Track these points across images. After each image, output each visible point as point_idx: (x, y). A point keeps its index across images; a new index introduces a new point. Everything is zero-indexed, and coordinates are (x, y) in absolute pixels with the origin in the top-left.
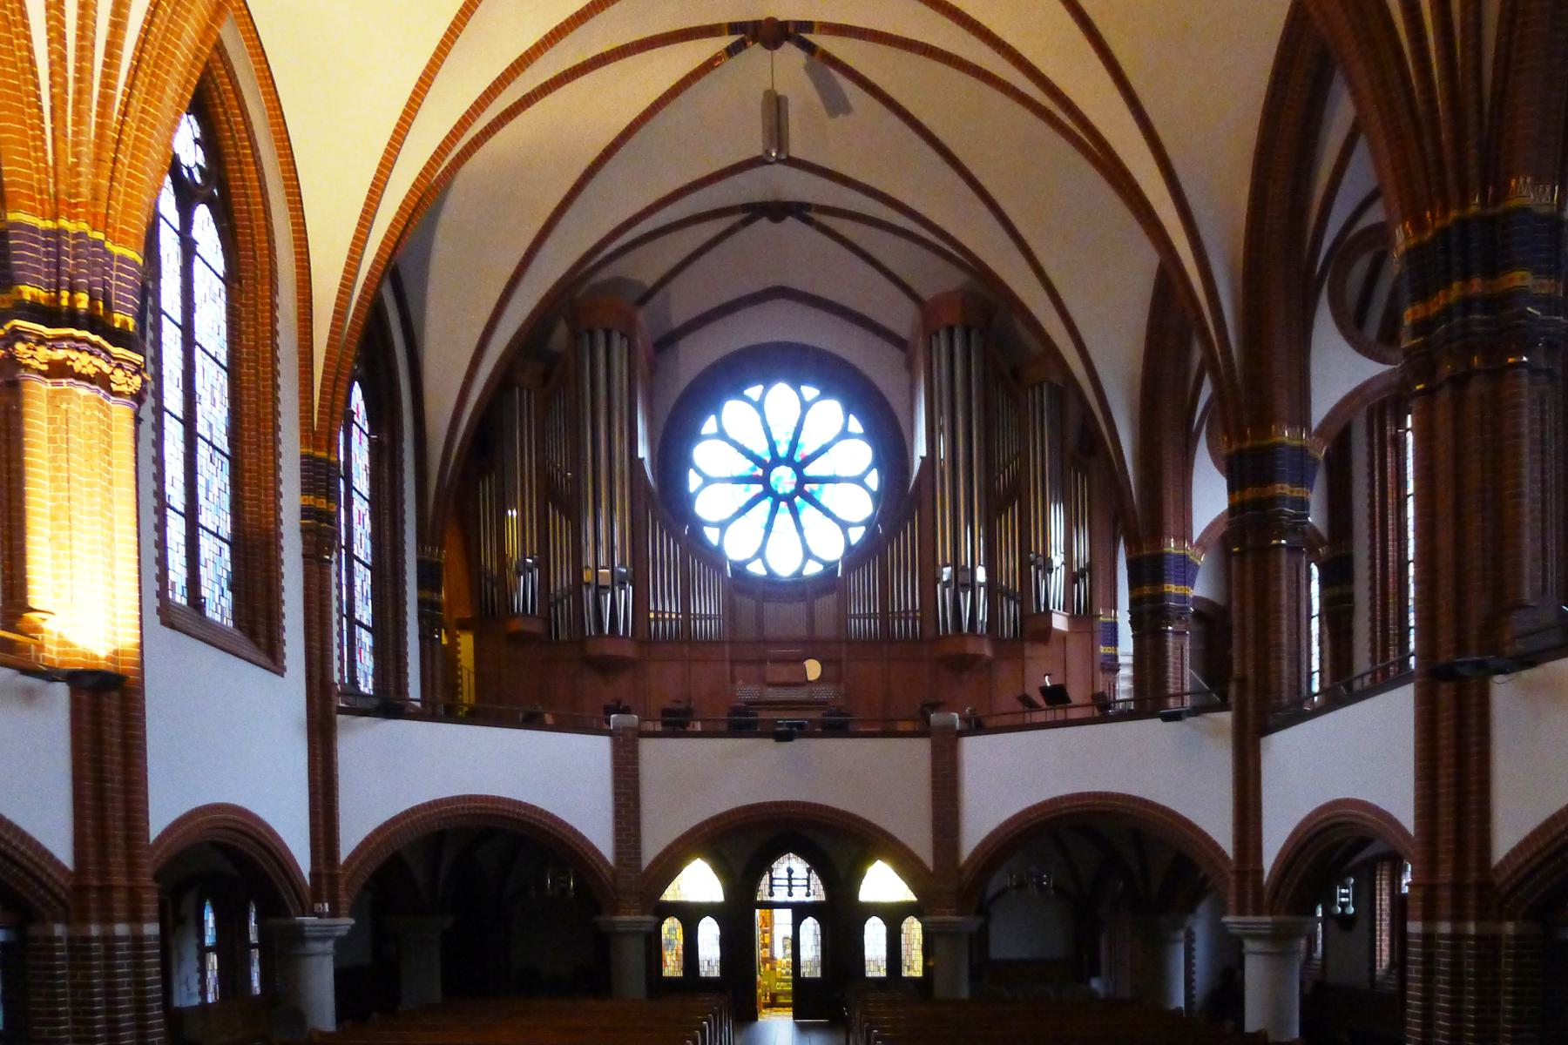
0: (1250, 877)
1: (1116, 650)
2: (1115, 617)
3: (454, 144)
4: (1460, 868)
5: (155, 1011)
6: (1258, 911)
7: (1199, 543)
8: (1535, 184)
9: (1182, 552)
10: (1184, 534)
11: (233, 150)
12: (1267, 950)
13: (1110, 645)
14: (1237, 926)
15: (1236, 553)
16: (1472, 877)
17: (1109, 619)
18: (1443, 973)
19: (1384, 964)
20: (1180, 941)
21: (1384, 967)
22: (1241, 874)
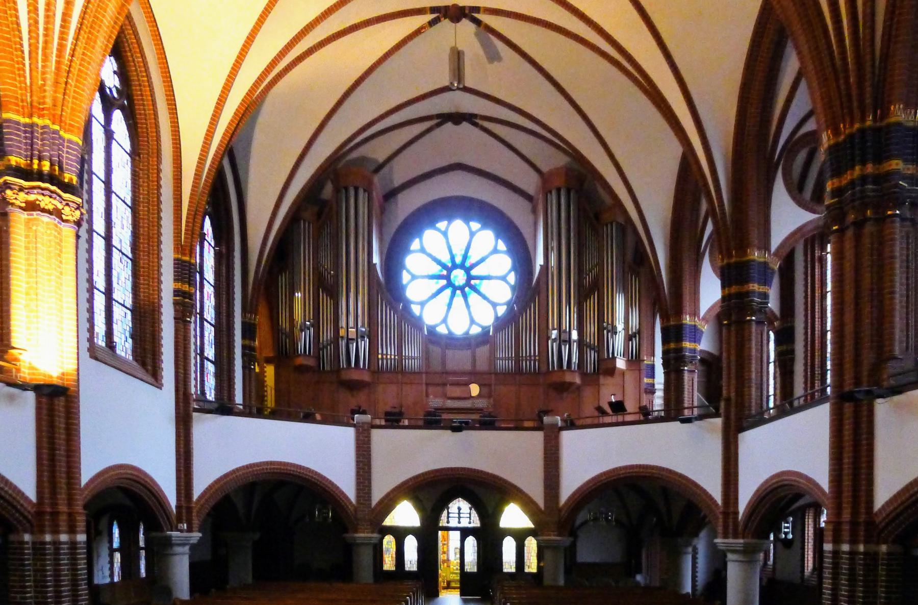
0: (731, 517)
4: (855, 513)
6: (736, 536)
13: (651, 378)
16: (862, 518)
20: (689, 553)
22: (726, 514)
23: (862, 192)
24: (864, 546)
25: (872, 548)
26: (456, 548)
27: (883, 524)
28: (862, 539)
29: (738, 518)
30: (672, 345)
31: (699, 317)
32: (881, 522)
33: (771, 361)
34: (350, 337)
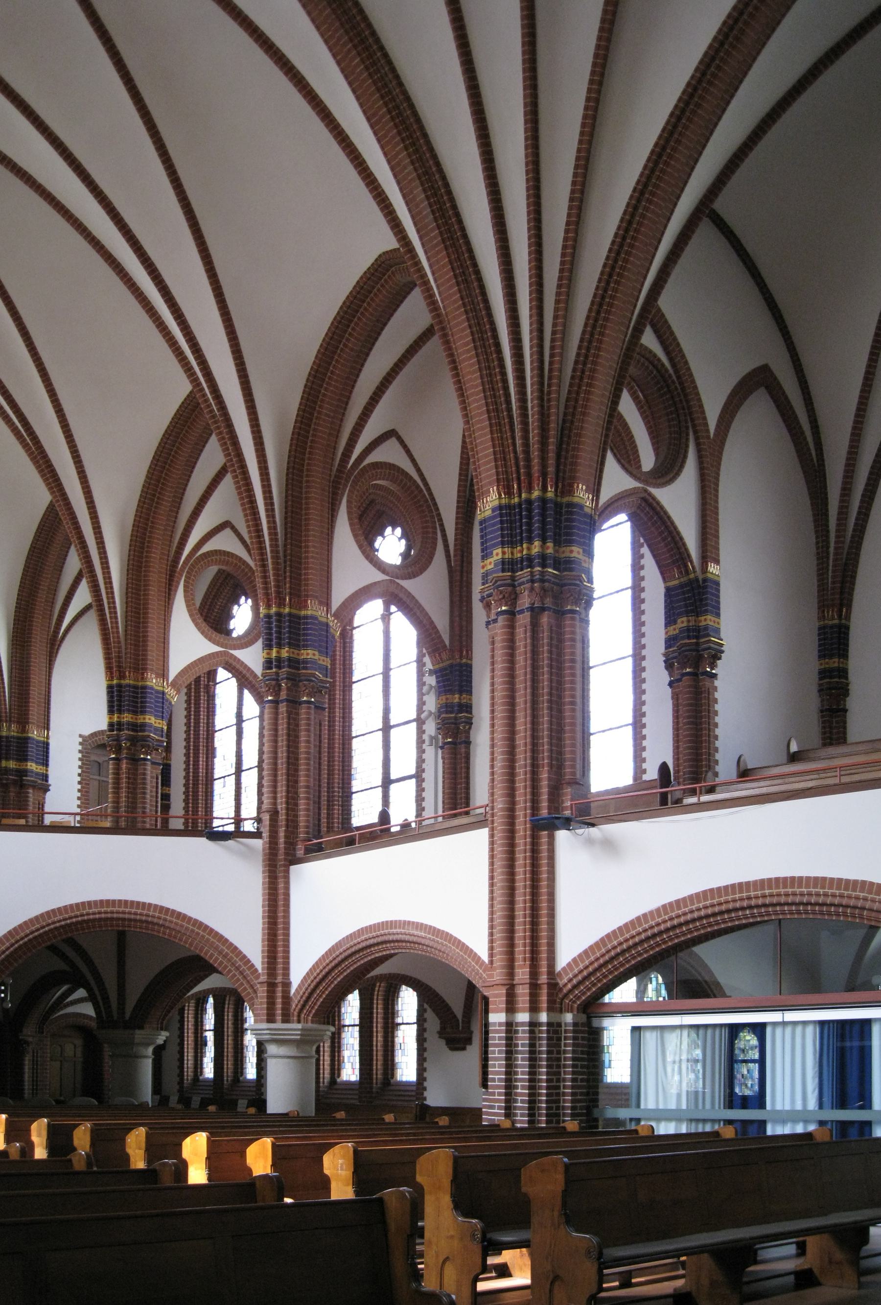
0: (280, 989)
1: (47, 771)
2: (48, 737)
3: (189, 363)
4: (534, 973)
5: (93, 983)
6: (286, 1019)
7: (174, 684)
8: (586, 491)
9: (161, 689)
10: (163, 674)
11: (713, 532)
12: (293, 1054)
13: (43, 764)
14: (268, 1032)
15: (270, 701)
16: (543, 979)
17: (42, 739)
18: (522, 1052)
19: (326, 1081)
20: (146, 1057)
21: (326, 1084)
22: (271, 986)
23: (542, 573)
24: (548, 1015)
25: (555, 1018)
26: (610, 1067)
27: (569, 986)
28: (545, 1005)
29: (289, 992)
30: (127, 717)
31: (168, 680)
32: (566, 985)
33: (255, 772)
34: (719, 205)
